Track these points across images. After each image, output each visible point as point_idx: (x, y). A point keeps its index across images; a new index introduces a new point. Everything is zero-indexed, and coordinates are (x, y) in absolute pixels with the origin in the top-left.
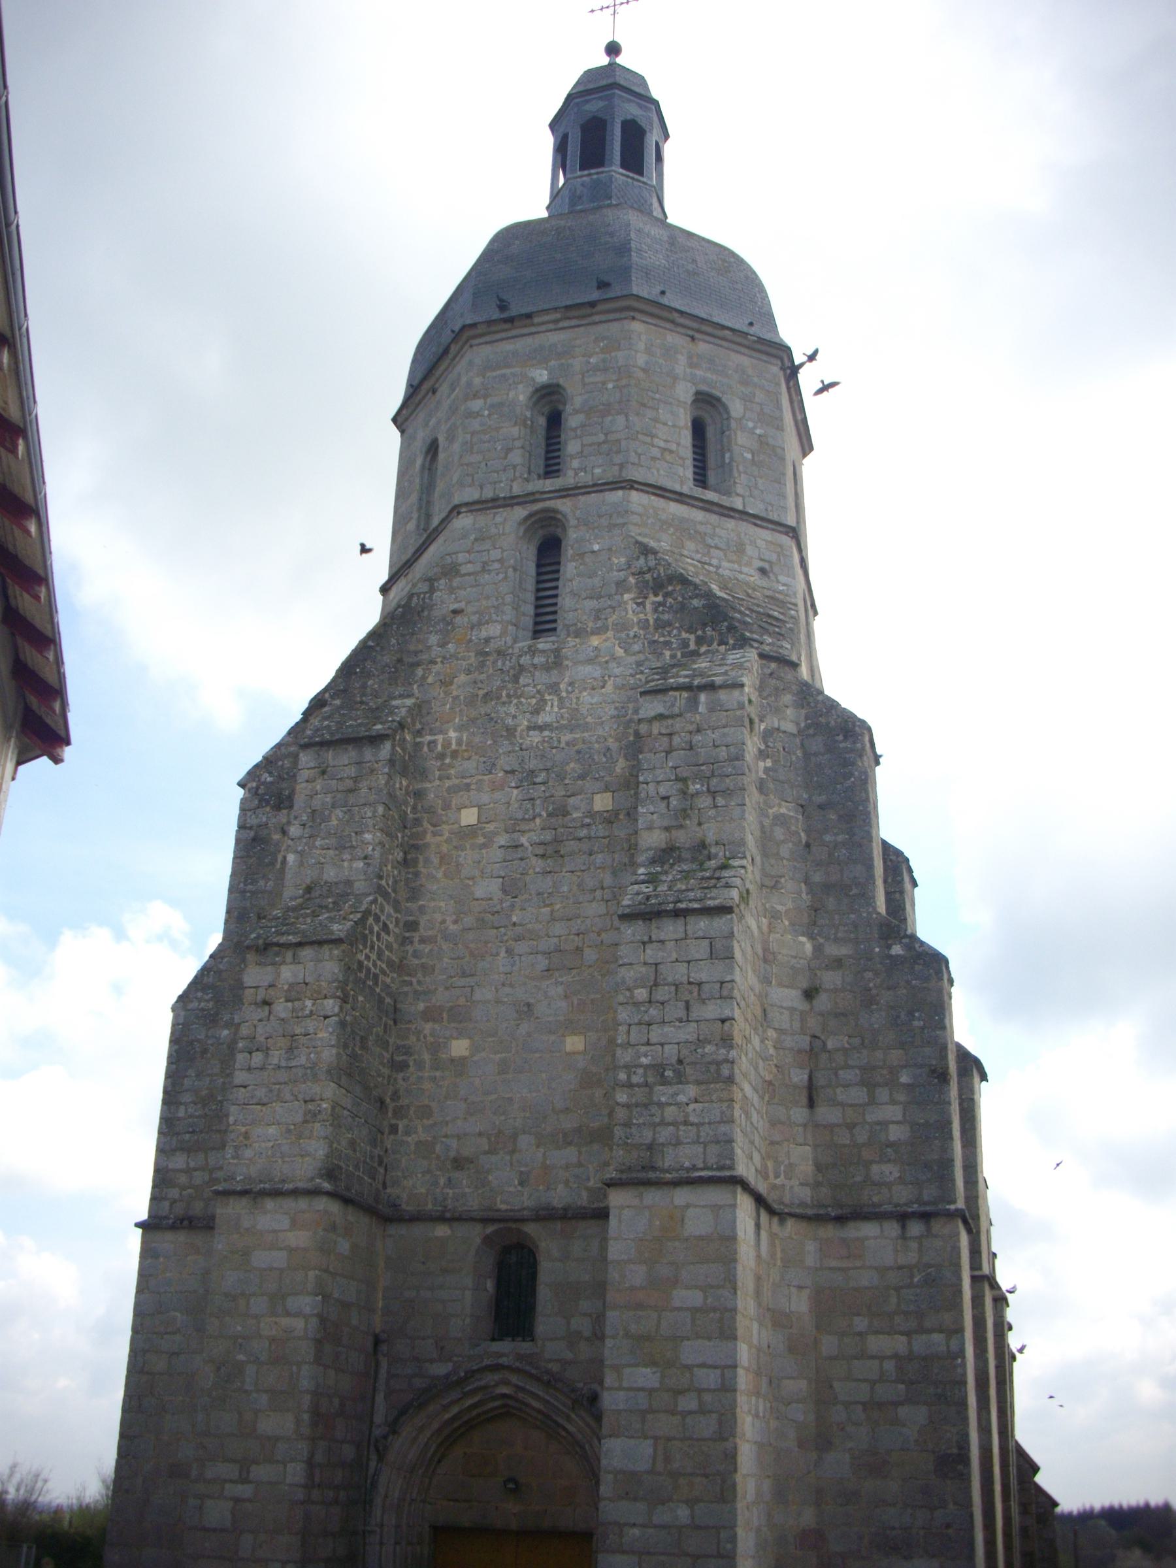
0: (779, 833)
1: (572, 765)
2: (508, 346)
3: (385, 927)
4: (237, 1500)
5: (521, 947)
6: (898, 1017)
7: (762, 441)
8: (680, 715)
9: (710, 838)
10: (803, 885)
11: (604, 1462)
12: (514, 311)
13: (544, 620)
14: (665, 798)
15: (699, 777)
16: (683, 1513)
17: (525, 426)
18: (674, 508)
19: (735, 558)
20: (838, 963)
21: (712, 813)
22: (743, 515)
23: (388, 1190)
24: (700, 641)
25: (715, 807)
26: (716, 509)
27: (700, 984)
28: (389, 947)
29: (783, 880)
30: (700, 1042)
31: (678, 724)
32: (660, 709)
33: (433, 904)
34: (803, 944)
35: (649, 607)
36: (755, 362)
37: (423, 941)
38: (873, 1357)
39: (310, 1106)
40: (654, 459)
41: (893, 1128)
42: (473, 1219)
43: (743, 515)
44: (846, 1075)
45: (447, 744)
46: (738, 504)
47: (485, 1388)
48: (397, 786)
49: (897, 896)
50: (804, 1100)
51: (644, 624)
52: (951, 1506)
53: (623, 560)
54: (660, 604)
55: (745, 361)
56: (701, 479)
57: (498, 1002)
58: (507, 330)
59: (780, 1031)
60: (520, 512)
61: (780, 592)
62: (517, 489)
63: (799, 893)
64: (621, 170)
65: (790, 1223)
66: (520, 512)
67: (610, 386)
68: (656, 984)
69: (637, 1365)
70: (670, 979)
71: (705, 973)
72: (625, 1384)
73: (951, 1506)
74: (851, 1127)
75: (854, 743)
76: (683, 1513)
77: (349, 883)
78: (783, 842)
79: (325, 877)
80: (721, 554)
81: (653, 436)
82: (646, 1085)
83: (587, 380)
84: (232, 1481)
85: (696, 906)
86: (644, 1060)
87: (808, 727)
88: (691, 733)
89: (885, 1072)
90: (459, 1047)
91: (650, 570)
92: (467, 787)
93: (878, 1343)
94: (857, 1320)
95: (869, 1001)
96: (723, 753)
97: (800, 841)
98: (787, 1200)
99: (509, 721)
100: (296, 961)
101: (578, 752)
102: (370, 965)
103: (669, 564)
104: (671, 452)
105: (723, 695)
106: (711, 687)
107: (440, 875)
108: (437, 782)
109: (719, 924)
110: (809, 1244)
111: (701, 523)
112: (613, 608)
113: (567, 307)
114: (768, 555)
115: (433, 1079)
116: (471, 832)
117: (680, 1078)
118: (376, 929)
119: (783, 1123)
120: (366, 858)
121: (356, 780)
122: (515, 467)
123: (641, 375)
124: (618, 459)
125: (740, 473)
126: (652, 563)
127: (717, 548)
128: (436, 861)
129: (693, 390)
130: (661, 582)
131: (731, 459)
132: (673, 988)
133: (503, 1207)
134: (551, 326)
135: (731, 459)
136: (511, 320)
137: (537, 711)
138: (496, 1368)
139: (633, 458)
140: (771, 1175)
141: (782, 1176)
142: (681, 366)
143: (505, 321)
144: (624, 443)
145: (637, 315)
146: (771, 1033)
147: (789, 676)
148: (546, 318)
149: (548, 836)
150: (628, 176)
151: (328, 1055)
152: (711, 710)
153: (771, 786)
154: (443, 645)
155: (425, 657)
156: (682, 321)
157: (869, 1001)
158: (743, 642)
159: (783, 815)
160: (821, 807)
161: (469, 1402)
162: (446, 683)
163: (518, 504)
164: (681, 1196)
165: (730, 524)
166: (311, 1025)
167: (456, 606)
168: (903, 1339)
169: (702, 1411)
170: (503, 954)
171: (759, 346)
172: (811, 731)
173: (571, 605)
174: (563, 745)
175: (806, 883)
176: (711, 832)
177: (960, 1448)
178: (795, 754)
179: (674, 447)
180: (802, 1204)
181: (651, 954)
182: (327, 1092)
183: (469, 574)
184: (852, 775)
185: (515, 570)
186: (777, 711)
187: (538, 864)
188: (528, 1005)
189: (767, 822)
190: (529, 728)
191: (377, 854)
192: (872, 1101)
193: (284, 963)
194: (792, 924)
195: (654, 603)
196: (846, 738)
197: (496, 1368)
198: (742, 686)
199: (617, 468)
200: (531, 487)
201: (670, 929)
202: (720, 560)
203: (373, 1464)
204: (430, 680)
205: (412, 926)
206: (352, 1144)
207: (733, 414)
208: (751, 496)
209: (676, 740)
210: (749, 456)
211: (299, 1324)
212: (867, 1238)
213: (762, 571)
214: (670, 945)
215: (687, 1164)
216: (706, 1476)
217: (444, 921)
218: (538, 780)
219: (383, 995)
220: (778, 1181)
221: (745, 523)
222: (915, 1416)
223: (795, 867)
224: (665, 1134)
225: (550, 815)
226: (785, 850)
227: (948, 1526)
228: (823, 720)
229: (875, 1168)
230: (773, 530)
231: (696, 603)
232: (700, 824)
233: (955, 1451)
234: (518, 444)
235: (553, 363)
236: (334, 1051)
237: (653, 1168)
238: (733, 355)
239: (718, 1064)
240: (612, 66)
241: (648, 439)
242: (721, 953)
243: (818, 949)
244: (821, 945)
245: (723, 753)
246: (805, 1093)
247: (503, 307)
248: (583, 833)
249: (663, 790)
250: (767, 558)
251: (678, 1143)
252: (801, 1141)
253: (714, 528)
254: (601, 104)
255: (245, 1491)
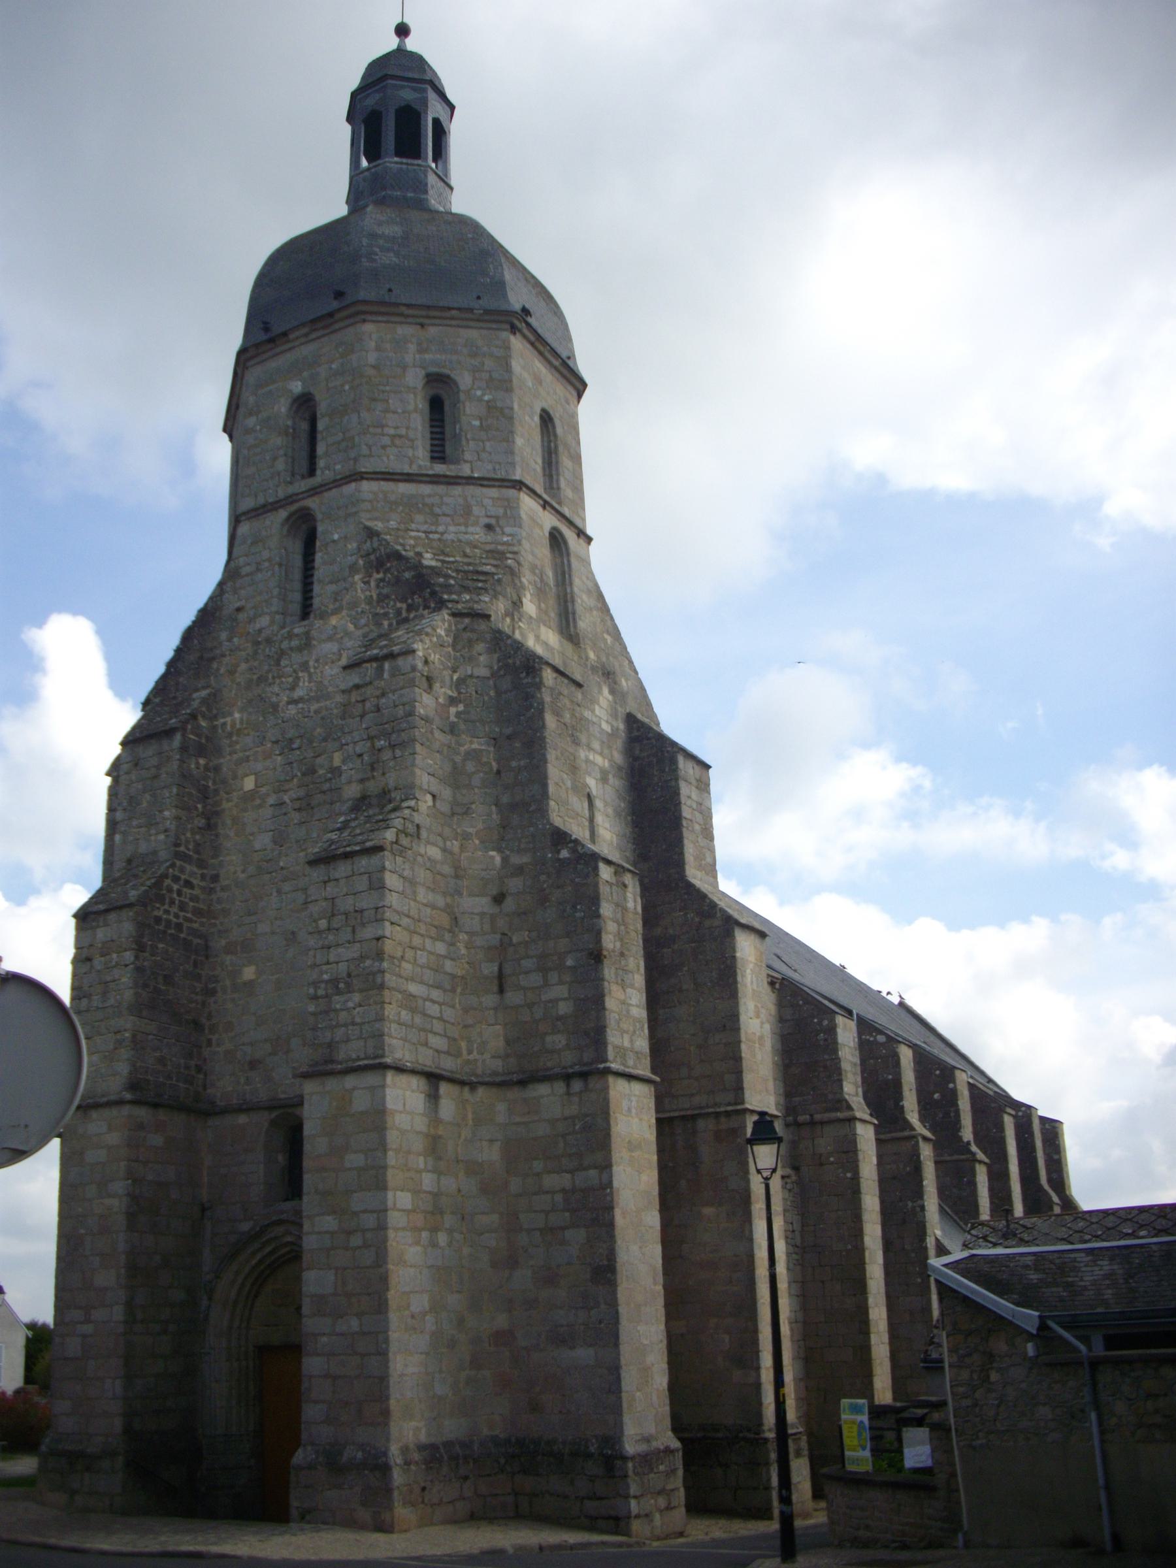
0: (470, 767)
1: (318, 730)
2: (273, 364)
3: (188, 884)
4: (84, 1336)
5: (287, 887)
6: (565, 911)
7: (491, 407)
8: (371, 683)
9: (391, 784)
10: (494, 808)
11: (304, 1289)
12: (277, 330)
13: (306, 611)
14: (360, 755)
15: (387, 735)
16: (354, 1324)
17: (287, 435)
18: (403, 488)
19: (462, 520)
20: (520, 870)
21: (392, 764)
22: (470, 480)
23: (209, 1091)
24: (410, 608)
25: (395, 758)
26: (442, 479)
27: (362, 911)
28: (194, 899)
29: (473, 806)
30: (362, 958)
31: (369, 691)
32: (357, 680)
33: (228, 858)
34: (492, 857)
35: (373, 584)
36: (484, 332)
37: (223, 889)
38: (547, 1192)
39: (118, 1037)
40: (384, 447)
41: (562, 1005)
42: (260, 1108)
43: (470, 480)
44: (527, 964)
45: (233, 724)
46: (466, 470)
47: (276, 1238)
48: (193, 766)
49: (673, 783)
50: (495, 989)
51: (369, 601)
52: (603, 1306)
53: (355, 545)
54: (382, 580)
55: (473, 334)
56: (439, 453)
57: (273, 933)
58: (271, 349)
59: (471, 934)
60: (283, 514)
61: (504, 544)
62: (281, 494)
63: (490, 815)
64: (396, 159)
65: (481, 1091)
66: (283, 514)
67: (347, 387)
68: (333, 915)
69: (323, 1214)
70: (342, 910)
71: (365, 902)
72: (316, 1229)
73: (603, 1306)
74: (530, 1006)
75: (534, 677)
76: (354, 1324)
77: (155, 853)
78: (474, 773)
79: (140, 851)
80: (448, 520)
81: (382, 426)
82: (327, 996)
83: (330, 385)
84: (81, 1323)
85: (357, 848)
86: (325, 977)
87: (500, 669)
88: (378, 697)
89: (555, 958)
90: (249, 973)
91: (374, 550)
92: (247, 759)
93: (552, 1181)
94: (536, 1163)
95: (543, 900)
96: (400, 712)
97: (491, 769)
98: (479, 1071)
99: (274, 699)
100: (106, 925)
101: (323, 718)
102: (171, 917)
103: (388, 543)
104: (400, 436)
105: (400, 661)
106: (391, 656)
107: (232, 834)
108: (228, 757)
109: (374, 860)
110: (501, 1107)
111: (430, 496)
112: (347, 589)
113: (313, 321)
114: (493, 511)
115: (233, 1000)
116: (250, 796)
117: (349, 989)
118: (175, 887)
119: (475, 1009)
120: (166, 831)
121: (158, 767)
122: (279, 474)
123: (372, 372)
124: (352, 455)
125: (467, 440)
126: (376, 545)
127: (445, 515)
128: (229, 822)
129: (423, 372)
130: (384, 560)
131: (461, 429)
132: (344, 917)
133: (283, 1096)
134: (303, 340)
135: (461, 429)
136: (271, 340)
137: (293, 688)
138: (280, 1222)
139: (365, 450)
140: (465, 1052)
141: (475, 1053)
142: (411, 354)
143: (271, 340)
144: (357, 439)
145: (369, 317)
146: (463, 937)
147: (482, 626)
148: (297, 334)
149: (302, 793)
150: (402, 163)
151: (128, 995)
152: (393, 675)
153: (462, 727)
154: (230, 640)
155: (218, 652)
156: (410, 312)
157: (543, 900)
158: (441, 604)
159: (474, 750)
160: (509, 737)
161: (268, 1249)
162: (232, 672)
163: (281, 507)
164: (350, 1081)
165: (457, 490)
166: (116, 973)
167: (238, 604)
168: (568, 1176)
169: (366, 1245)
170: (275, 894)
171: (486, 318)
172: (502, 673)
173: (322, 593)
174: (312, 714)
175: (496, 805)
176: (391, 780)
177: (609, 1260)
178: (488, 695)
179: (403, 431)
180: (495, 1073)
181: (330, 890)
182: (128, 1023)
183: (247, 575)
184: (531, 706)
185: (280, 565)
186: (471, 659)
187: (296, 817)
188: (293, 933)
189: (458, 759)
190: (289, 703)
191: (173, 827)
192: (546, 984)
193: (98, 926)
194: (482, 842)
195: (377, 580)
196: (528, 674)
197: (280, 1222)
198: (414, 651)
199: (352, 462)
200: (291, 490)
201: (342, 869)
202: (433, 530)
203: (205, 1302)
204: (222, 671)
205: (215, 878)
206: (162, 1061)
207: (462, 388)
208: (479, 459)
209: (368, 705)
210: (477, 423)
211: (115, 1202)
212: (542, 1097)
213: (489, 527)
214: (342, 882)
215: (354, 1056)
216: (369, 1294)
217: (235, 873)
218: (295, 746)
219: (190, 938)
220: (471, 1057)
221: (472, 487)
222: (576, 1236)
223: (486, 793)
224: (340, 1033)
225: (304, 774)
226: (476, 780)
227: (600, 1322)
228: (510, 661)
229: (549, 1039)
230: (500, 486)
231: (407, 575)
232: (384, 774)
233: (605, 1263)
234: (281, 452)
235: (305, 374)
236: (132, 991)
237: (332, 1061)
238: (462, 332)
239: (374, 974)
240: (400, 51)
241: (379, 430)
242: (378, 886)
243: (505, 860)
244: (508, 856)
245: (400, 712)
246: (496, 982)
247: (266, 329)
248: (326, 786)
249: (358, 750)
250: (493, 513)
251: (348, 1041)
252: (492, 1022)
253: (441, 497)
254: (378, 96)
255: (88, 1329)
